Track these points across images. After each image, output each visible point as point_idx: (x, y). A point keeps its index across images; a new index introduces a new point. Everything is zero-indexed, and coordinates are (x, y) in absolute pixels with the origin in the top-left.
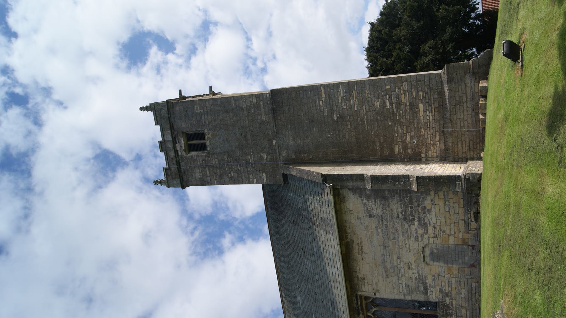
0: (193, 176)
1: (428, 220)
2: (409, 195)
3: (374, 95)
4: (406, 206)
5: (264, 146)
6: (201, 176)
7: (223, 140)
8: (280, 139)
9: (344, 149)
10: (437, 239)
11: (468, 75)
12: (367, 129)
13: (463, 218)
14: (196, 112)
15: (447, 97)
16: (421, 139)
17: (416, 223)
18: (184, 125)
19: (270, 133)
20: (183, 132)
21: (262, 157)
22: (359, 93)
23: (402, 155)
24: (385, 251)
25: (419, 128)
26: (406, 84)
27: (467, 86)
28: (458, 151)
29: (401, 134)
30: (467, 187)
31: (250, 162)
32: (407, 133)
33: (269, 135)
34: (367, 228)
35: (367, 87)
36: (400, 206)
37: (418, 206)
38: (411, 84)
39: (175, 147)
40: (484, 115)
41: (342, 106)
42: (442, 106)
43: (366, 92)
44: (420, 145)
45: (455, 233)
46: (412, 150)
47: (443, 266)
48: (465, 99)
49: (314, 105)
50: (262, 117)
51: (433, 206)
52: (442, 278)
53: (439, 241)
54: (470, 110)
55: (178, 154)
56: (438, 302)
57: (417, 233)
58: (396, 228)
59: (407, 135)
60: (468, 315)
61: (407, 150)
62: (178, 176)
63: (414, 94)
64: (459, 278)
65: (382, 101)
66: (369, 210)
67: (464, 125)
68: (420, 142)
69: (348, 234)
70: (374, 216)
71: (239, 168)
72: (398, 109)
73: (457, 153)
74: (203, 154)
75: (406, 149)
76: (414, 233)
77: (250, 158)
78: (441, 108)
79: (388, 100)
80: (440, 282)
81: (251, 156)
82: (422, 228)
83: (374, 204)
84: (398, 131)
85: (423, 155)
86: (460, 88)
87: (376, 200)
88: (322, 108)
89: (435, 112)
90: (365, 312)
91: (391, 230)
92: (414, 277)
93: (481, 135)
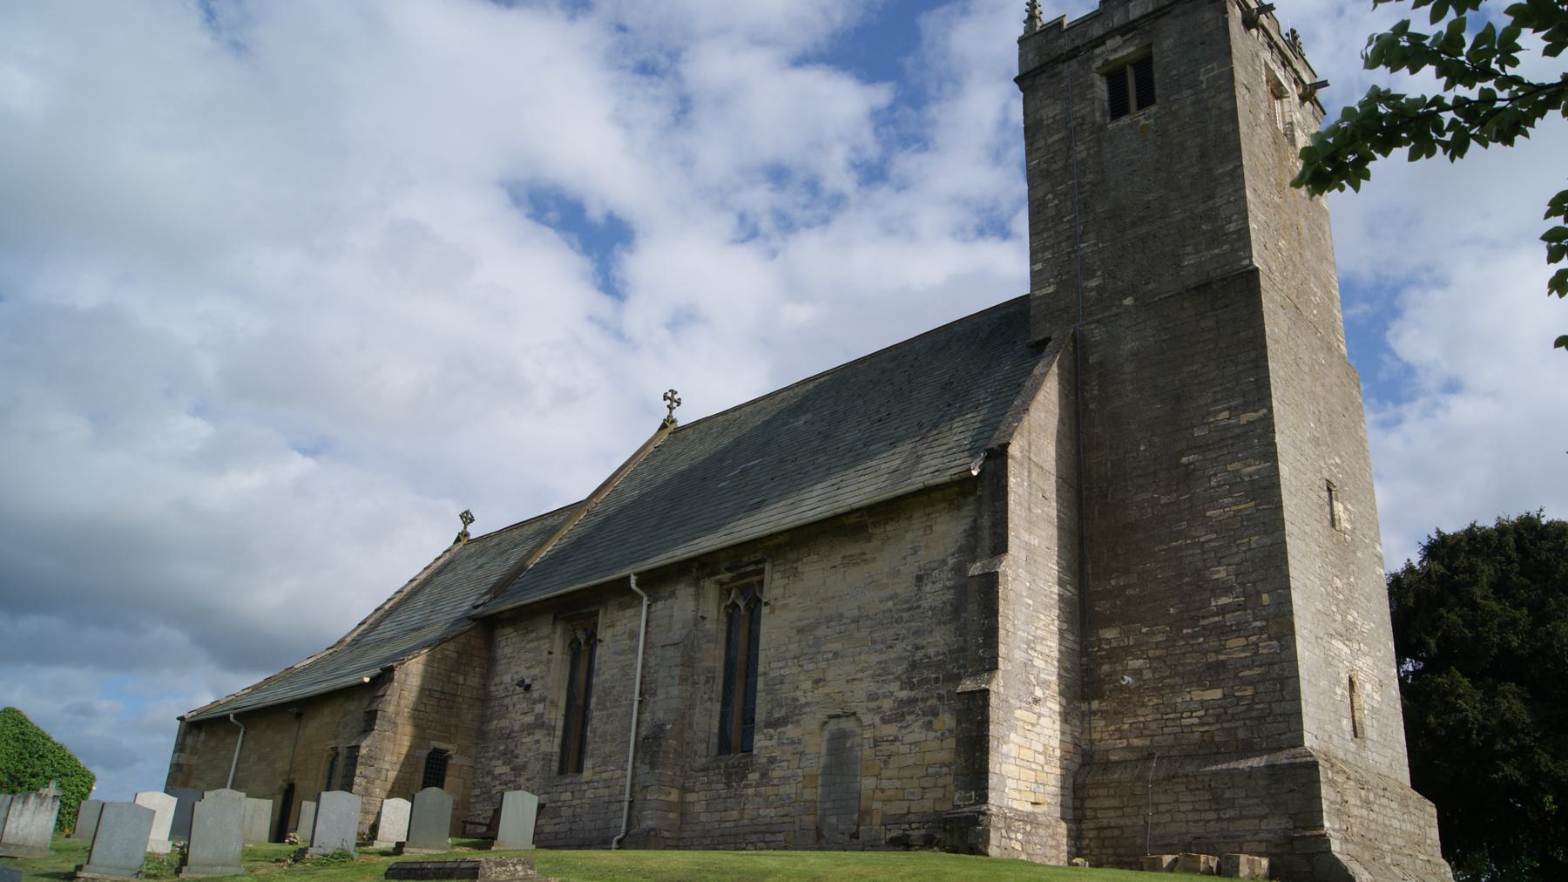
0: (1046, 100)
1: (910, 722)
3: (1246, 561)
5: (1120, 276)
6: (1045, 122)
7: (1132, 160)
8: (1135, 316)
9: (1110, 492)
10: (872, 746)
11: (1291, 825)
12: (1160, 551)
14: (1202, 70)
15: (1233, 765)
16: (1135, 699)
17: (904, 694)
18: (1167, 44)
19: (1150, 287)
20: (1150, 45)
21: (1091, 274)
22: (1249, 518)
23: (1096, 649)
24: (849, 621)
25: (1163, 692)
26: (1274, 648)
27: (1261, 821)
28: (1098, 796)
29: (1147, 642)
30: (958, 818)
31: (1082, 245)
32: (1148, 658)
33: (1147, 283)
35: (1267, 541)
38: (1273, 664)
39: (1110, 34)
40: (1171, 868)
41: (1215, 475)
42: (1217, 753)
43: (1254, 539)
44: (1121, 697)
45: (883, 791)
46: (1107, 676)
47: (819, 763)
48: (1227, 816)
49: (1219, 396)
50: (1190, 257)
51: (939, 734)
52: (794, 763)
53: (868, 752)
54: (1198, 830)
56: (752, 755)
57: (885, 697)
58: (895, 644)
59: (1146, 659)
60: (728, 825)
61: (1107, 660)
62: (1045, 59)
63: (1247, 673)
65: (1228, 585)
66: (931, 574)
67: (1162, 813)
68: (1127, 695)
69: (883, 526)
70: (919, 587)
71: (1065, 219)
72: (1208, 631)
73: (1096, 794)
74: (1098, 114)
75: (1110, 659)
76: (884, 690)
77: (1091, 242)
78: (1210, 750)
79: (1231, 600)
81: (1096, 245)
82: (895, 709)
83: (945, 586)
84: (1153, 634)
85: (1095, 705)
86: (1256, 801)
87: (952, 591)
88: (1212, 420)
89: (1201, 732)
90: (737, 584)
91: (891, 632)
92: (799, 693)
93: (1134, 859)
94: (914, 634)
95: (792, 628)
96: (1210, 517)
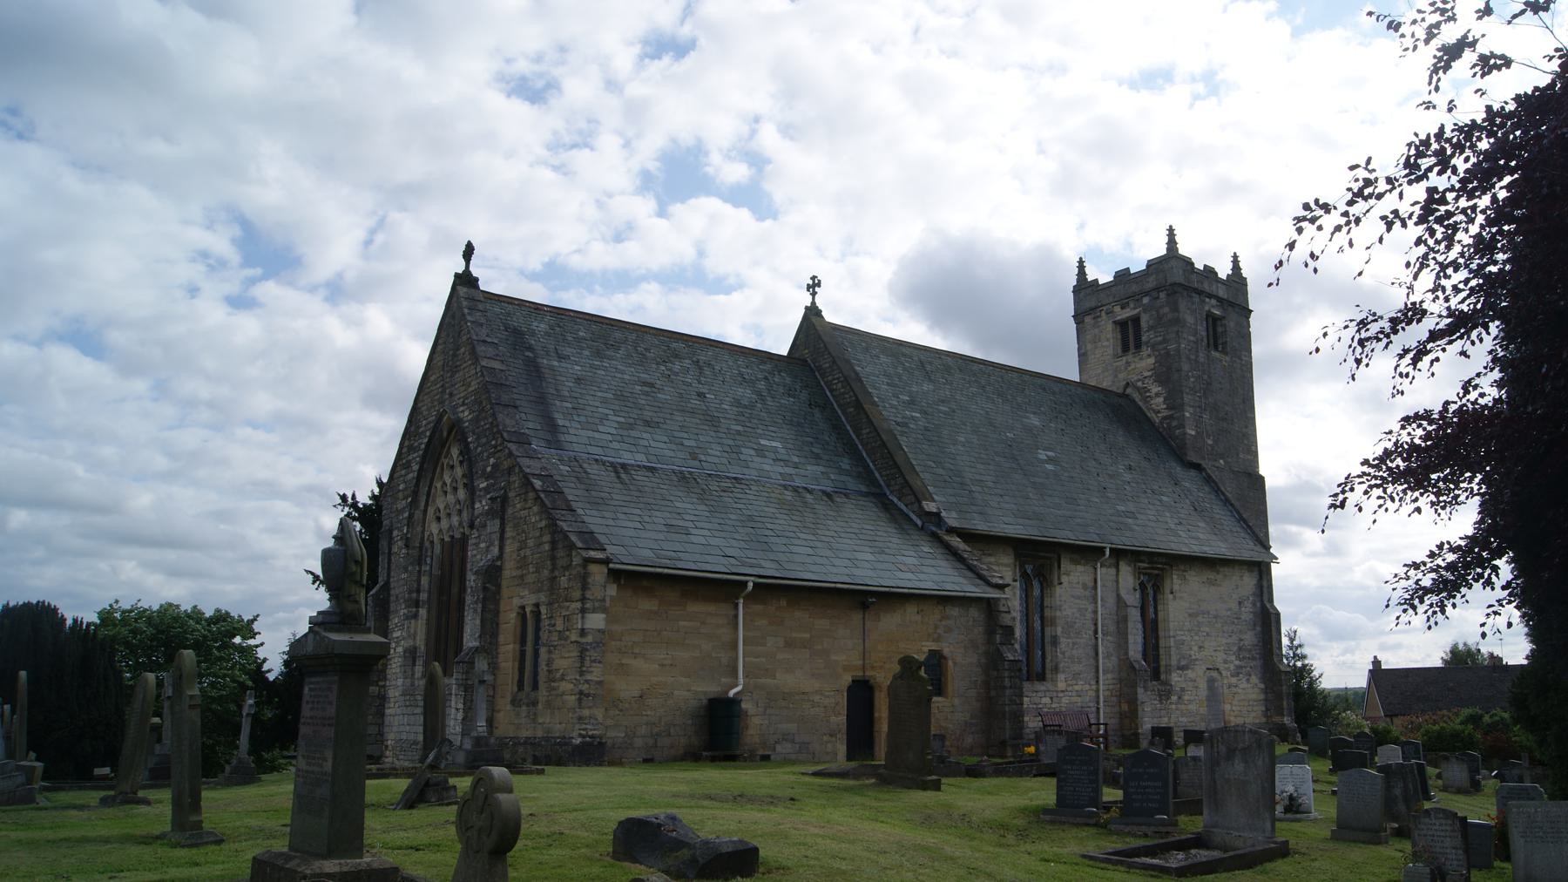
4: (1250, 651)
17: (1237, 663)
21: (1209, 437)
45: (1234, 711)
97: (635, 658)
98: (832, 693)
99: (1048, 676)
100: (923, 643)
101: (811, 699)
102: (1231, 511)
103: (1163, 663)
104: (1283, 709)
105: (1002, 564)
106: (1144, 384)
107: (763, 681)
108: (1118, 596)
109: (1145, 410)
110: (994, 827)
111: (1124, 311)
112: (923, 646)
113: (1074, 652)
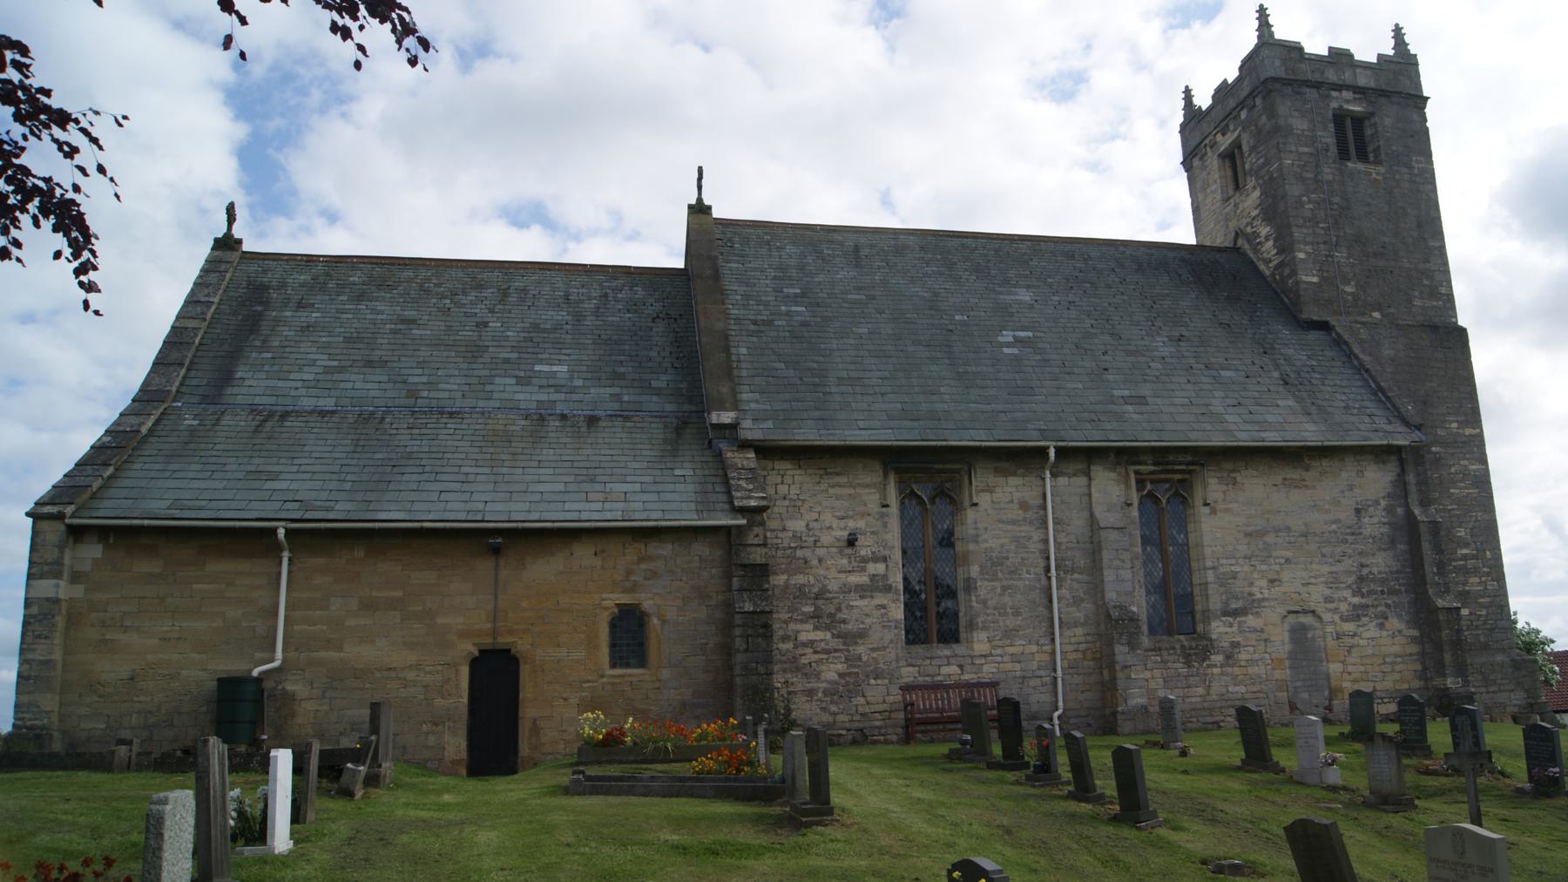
2: (1403, 589)
4: (1383, 581)
13: (1378, 688)
17: (1356, 600)
21: (1348, 282)
34: (1336, 503)
36: (1383, 570)
37: (1388, 606)
38: (1495, 596)
43: (1479, 514)
45: (1350, 673)
51: (1391, 633)
53: (1331, 643)
55: (1335, 90)
60: (1194, 700)
64: (1267, 680)
71: (1321, 225)
80: (1254, 643)
91: (1338, 550)
92: (1255, 590)
94: (1360, 554)
95: (1239, 531)
96: (1453, 494)
97: (125, 632)
98: (440, 668)
99: (963, 635)
100: (604, 596)
101: (400, 675)
102: (1366, 380)
103: (1198, 608)
104: (1444, 666)
105: (860, 485)
106: (1252, 228)
107: (322, 654)
108: (1092, 515)
109: (1255, 260)
110: (934, 844)
111: (1227, 136)
112: (604, 600)
113: (1007, 599)
